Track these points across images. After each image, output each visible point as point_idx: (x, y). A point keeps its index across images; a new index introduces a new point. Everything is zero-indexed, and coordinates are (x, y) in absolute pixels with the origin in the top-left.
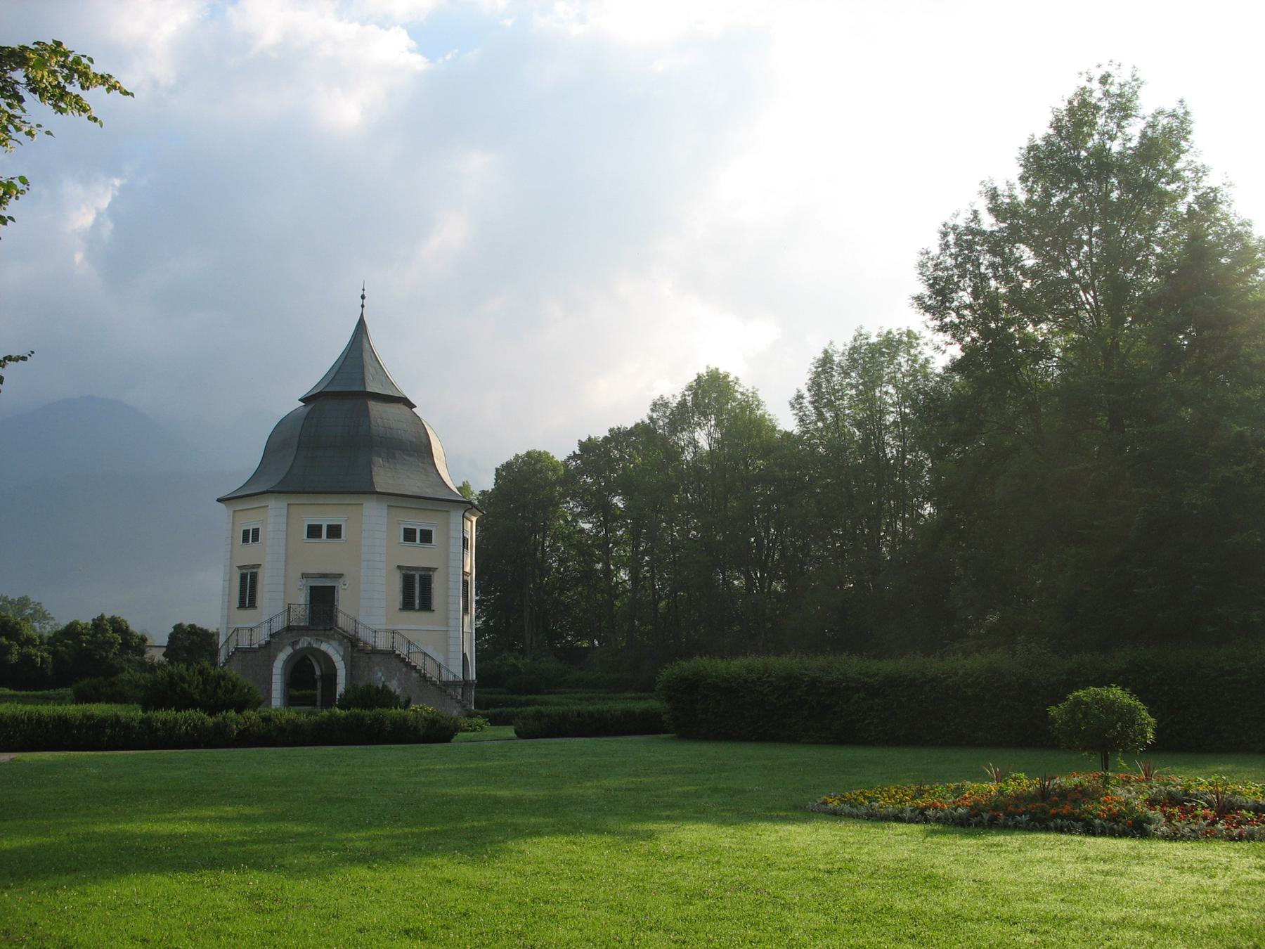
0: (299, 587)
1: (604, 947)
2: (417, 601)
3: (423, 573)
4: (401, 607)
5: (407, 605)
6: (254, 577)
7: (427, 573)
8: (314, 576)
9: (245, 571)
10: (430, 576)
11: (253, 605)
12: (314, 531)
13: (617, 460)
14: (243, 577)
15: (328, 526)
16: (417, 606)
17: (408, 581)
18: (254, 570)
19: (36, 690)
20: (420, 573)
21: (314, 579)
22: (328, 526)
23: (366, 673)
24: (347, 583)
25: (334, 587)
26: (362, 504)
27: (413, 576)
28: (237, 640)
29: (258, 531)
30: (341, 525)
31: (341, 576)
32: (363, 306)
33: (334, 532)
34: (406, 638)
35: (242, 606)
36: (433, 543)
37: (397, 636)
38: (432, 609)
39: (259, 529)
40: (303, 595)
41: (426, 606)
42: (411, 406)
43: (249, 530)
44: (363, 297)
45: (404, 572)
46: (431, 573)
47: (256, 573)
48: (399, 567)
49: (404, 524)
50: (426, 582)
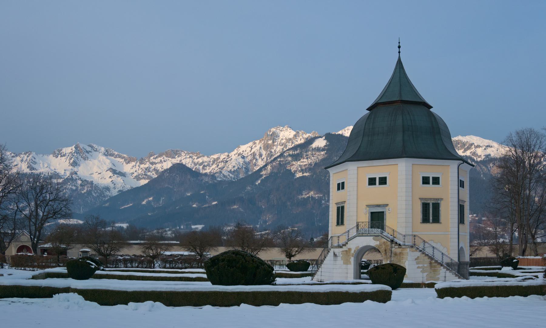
2: (431, 218)
3: (434, 202)
4: (422, 222)
5: (425, 220)
6: (343, 208)
7: (436, 202)
8: (374, 206)
9: (339, 206)
10: (439, 204)
11: (342, 223)
12: (372, 182)
14: (338, 208)
15: (380, 178)
16: (431, 221)
17: (425, 206)
18: (343, 205)
20: (341, 205)
22: (380, 178)
23: (522, 192)
24: (390, 209)
25: (383, 212)
26: (398, 164)
28: (332, 242)
29: (439, 179)
31: (387, 205)
32: (399, 52)
33: (383, 181)
34: (422, 239)
35: (338, 224)
37: (417, 238)
38: (440, 222)
44: (399, 47)
45: (423, 202)
46: (439, 202)
47: (344, 206)
50: (436, 207)
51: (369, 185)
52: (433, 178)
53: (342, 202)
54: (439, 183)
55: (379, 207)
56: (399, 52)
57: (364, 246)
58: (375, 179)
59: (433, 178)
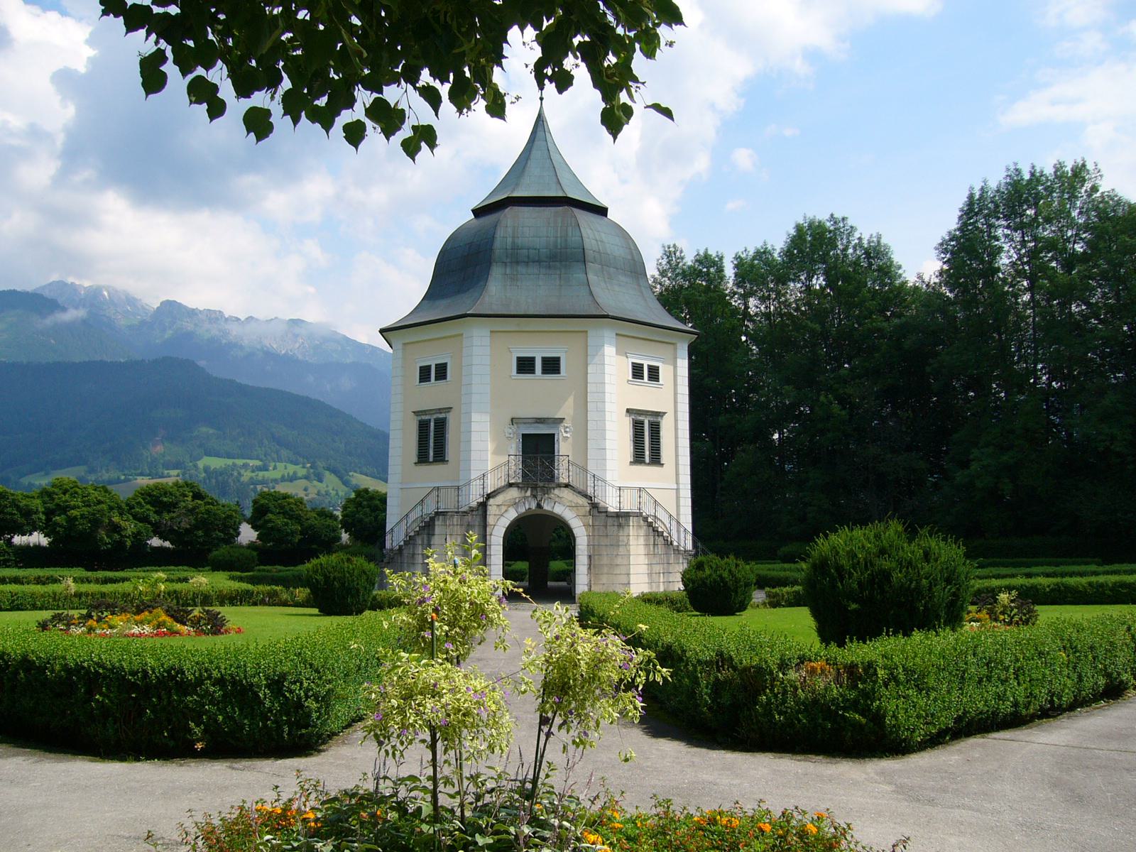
0: (507, 435)
1: (1133, 833)
2: (647, 453)
6: (441, 425)
8: (530, 421)
11: (440, 457)
12: (525, 365)
13: (1086, 318)
14: (423, 427)
16: (647, 460)
19: (242, 572)
20: (435, 416)
21: (528, 425)
26: (462, 335)
27: (642, 423)
29: (446, 367)
30: (559, 358)
32: (541, 99)
33: (552, 366)
35: (422, 458)
36: (661, 382)
37: (643, 494)
39: (446, 364)
40: (514, 446)
41: (656, 460)
42: (602, 211)
43: (430, 366)
48: (628, 411)
49: (633, 357)
51: (543, 373)
52: (545, 360)
53: (440, 409)
54: (420, 370)
55: (542, 423)
56: (541, 99)
57: (563, 515)
58: (532, 360)
59: (545, 360)
